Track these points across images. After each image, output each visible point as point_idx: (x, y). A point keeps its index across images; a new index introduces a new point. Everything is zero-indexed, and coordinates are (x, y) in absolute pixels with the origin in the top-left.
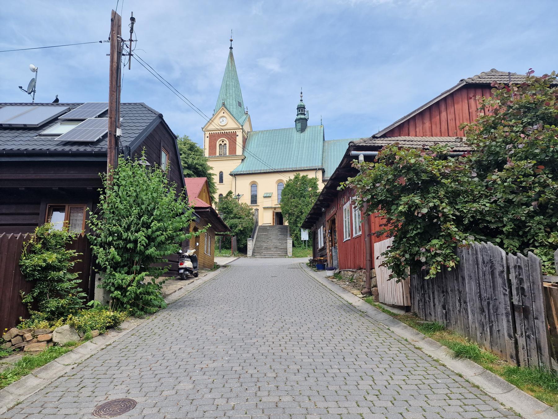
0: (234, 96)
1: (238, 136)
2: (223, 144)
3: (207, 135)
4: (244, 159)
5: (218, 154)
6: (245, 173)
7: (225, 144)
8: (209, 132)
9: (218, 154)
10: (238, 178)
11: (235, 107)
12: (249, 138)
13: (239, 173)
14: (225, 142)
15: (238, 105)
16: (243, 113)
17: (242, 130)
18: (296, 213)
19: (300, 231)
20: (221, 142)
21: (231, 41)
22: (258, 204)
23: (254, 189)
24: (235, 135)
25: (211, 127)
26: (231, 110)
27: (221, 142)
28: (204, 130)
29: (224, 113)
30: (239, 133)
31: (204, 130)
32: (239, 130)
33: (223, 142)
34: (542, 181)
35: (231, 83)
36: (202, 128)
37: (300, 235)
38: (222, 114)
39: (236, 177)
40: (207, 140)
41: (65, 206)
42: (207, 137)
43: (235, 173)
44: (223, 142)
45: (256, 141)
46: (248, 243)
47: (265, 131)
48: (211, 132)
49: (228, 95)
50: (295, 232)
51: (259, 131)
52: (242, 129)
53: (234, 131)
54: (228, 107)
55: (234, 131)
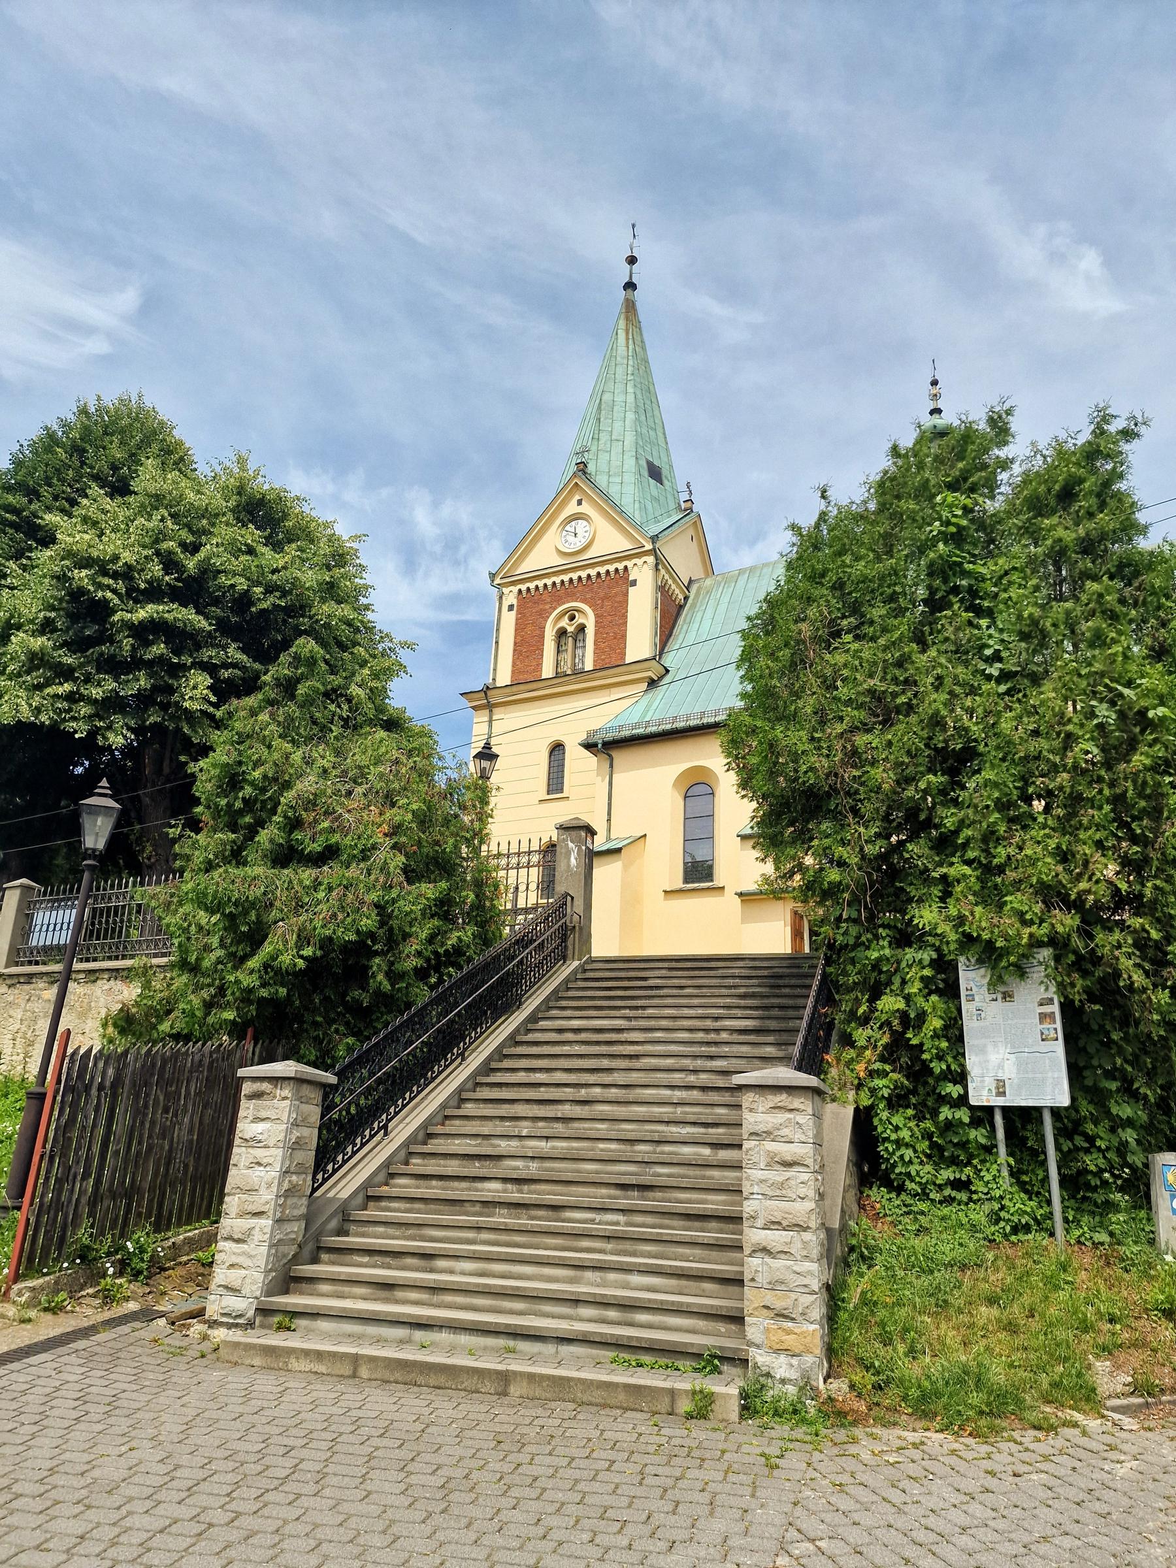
0: (630, 439)
1: (634, 583)
2: (570, 629)
3: (511, 598)
4: (661, 678)
5: (548, 671)
6: (653, 729)
7: (582, 629)
8: (515, 589)
9: (548, 671)
10: (620, 756)
11: (630, 478)
12: (694, 605)
13: (626, 733)
14: (580, 619)
15: (646, 473)
16: (672, 505)
17: (651, 559)
18: (882, 775)
19: (951, 991)
20: (564, 623)
21: (632, 260)
22: (717, 882)
23: (698, 806)
24: (624, 580)
25: (531, 564)
26: (614, 491)
27: (564, 623)
28: (498, 581)
29: (580, 503)
30: (643, 574)
31: (498, 581)
32: (639, 561)
33: (572, 618)
34: (944, 1044)
35: (619, 398)
36: (493, 576)
37: (954, 1032)
38: (572, 508)
39: (614, 754)
40: (509, 620)
41: (985, 1046)
42: (511, 608)
43: (609, 737)
44: (572, 618)
45: (723, 607)
46: (246, 1127)
47: (765, 565)
48: (523, 587)
49: (604, 437)
50: (890, 1003)
51: (741, 572)
52: (653, 552)
53: (620, 566)
54: (601, 480)
55: (620, 566)
